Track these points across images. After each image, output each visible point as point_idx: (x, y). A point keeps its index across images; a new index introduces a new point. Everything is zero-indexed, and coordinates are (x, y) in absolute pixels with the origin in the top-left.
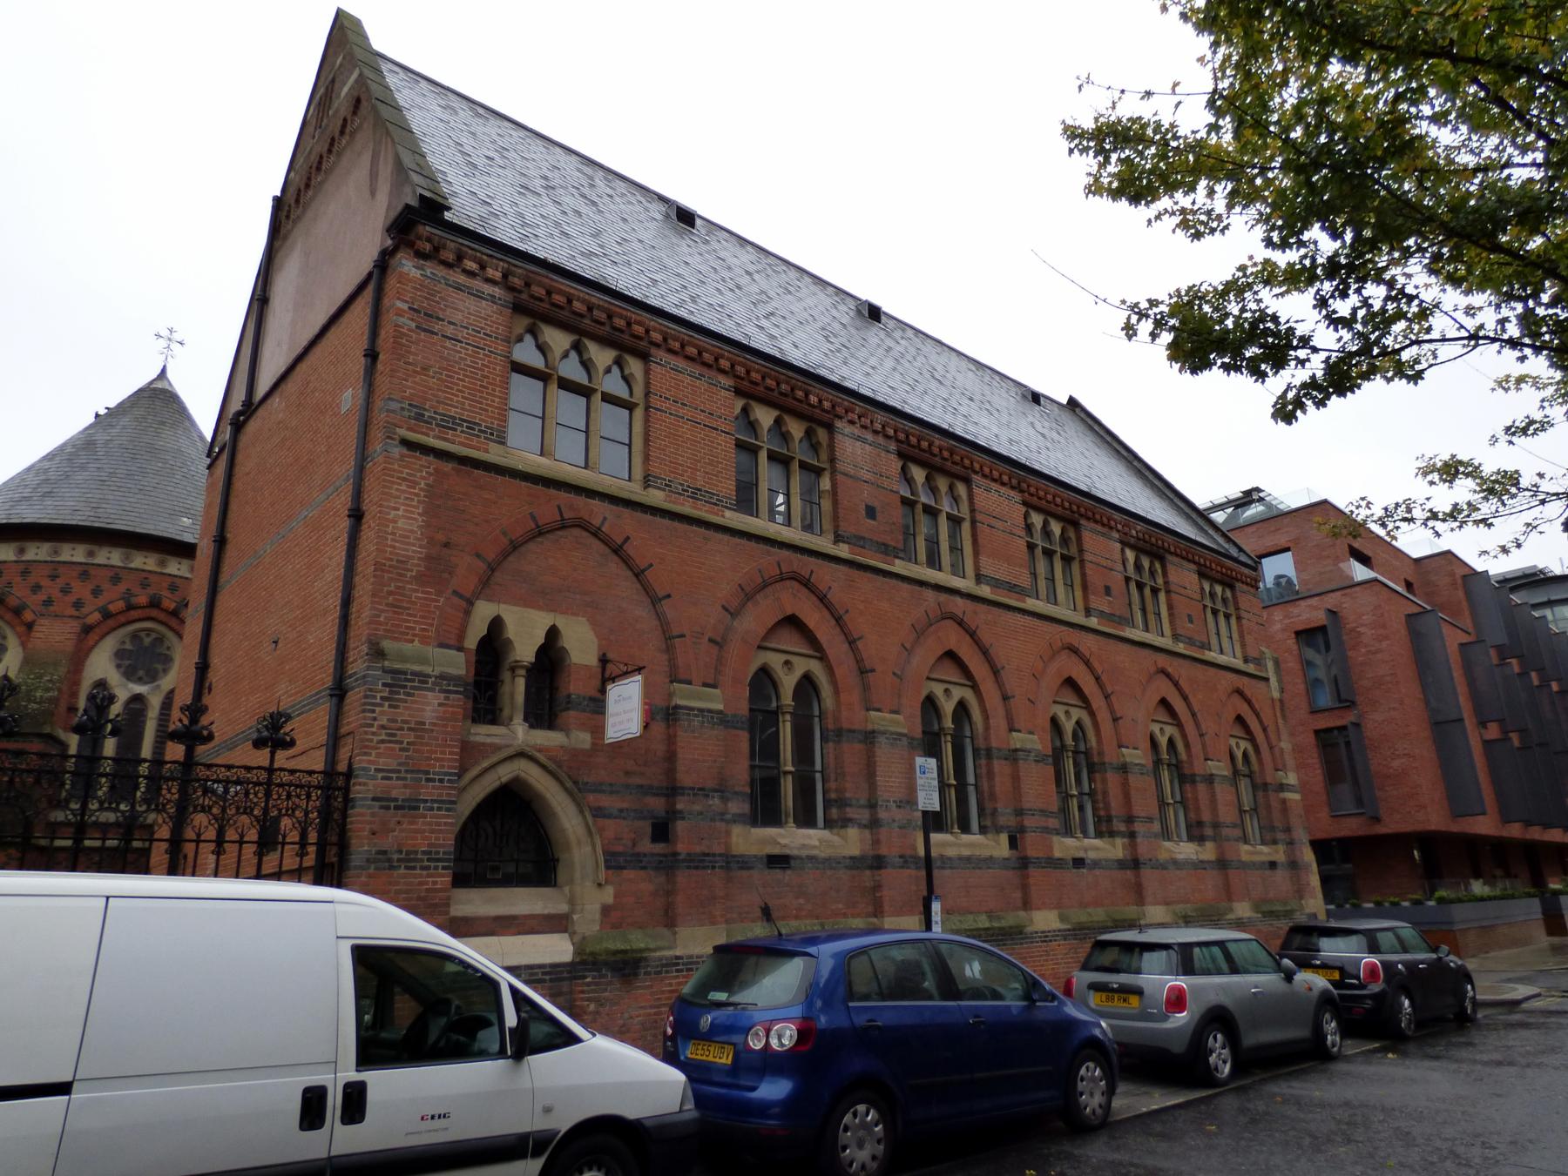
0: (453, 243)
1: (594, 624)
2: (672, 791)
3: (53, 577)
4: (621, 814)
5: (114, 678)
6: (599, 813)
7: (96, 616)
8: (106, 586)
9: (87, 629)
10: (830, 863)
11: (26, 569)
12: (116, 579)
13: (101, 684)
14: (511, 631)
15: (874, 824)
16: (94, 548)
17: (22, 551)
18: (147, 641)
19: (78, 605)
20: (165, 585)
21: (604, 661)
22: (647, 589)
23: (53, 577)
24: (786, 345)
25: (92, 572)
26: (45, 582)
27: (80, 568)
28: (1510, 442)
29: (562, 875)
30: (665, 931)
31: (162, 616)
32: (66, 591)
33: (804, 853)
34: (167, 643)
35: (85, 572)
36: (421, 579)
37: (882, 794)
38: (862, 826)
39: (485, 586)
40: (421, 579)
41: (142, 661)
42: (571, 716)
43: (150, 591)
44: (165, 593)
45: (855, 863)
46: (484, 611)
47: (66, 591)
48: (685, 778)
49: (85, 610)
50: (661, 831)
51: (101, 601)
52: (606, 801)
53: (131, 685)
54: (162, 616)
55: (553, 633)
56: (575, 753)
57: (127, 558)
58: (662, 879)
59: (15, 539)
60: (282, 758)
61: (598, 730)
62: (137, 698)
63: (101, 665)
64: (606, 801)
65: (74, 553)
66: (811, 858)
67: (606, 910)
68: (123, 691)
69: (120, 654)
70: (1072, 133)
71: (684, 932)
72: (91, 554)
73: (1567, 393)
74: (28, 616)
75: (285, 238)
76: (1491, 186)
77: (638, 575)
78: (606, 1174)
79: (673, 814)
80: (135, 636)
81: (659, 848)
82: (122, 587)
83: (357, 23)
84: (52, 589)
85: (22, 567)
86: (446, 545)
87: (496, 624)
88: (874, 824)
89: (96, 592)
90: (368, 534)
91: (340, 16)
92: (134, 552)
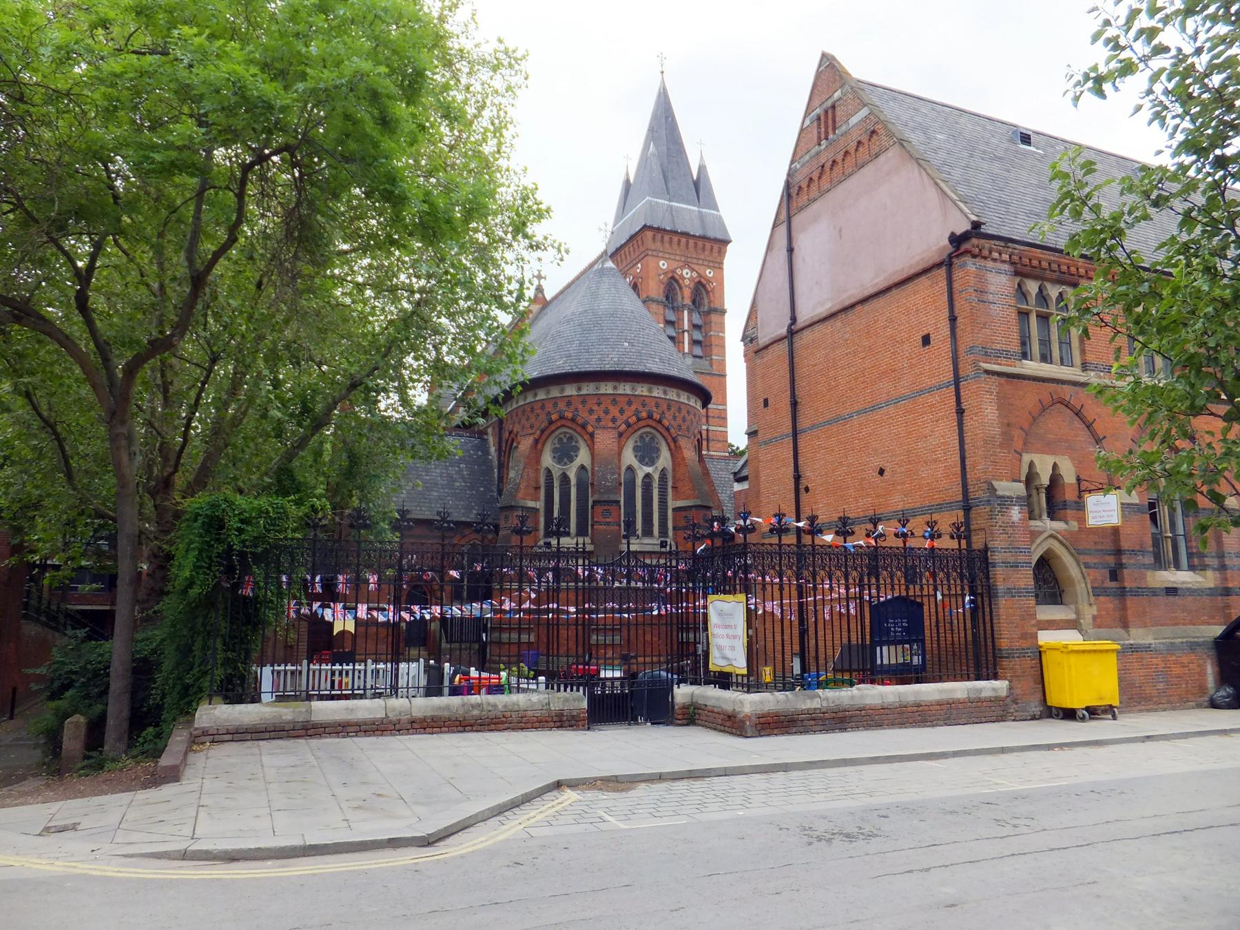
0: (987, 244)
1: (1072, 459)
2: (1118, 552)
3: (599, 404)
4: (1095, 567)
5: (635, 463)
6: (1087, 566)
7: (624, 426)
8: (626, 407)
9: (621, 435)
10: (1191, 592)
11: (584, 399)
12: (630, 403)
13: (630, 469)
14: (1038, 468)
15: (1223, 568)
16: (616, 384)
17: (579, 389)
18: (647, 439)
19: (614, 420)
21: (1078, 479)
22: (1094, 434)
23: (599, 404)
26: (595, 408)
29: (1066, 598)
30: (1121, 631)
31: (654, 424)
33: (1184, 586)
35: (614, 399)
36: (1001, 446)
37: (1227, 549)
38: (1214, 569)
39: (1027, 446)
40: (1001, 446)
41: (647, 454)
42: (1070, 513)
45: (1212, 592)
46: (1027, 458)
47: (607, 412)
48: (1125, 545)
49: (618, 423)
50: (1114, 575)
51: (625, 417)
52: (1088, 559)
54: (654, 424)
55: (1055, 466)
56: (1071, 533)
57: (650, 390)
58: (1117, 602)
61: (1082, 520)
62: (648, 476)
63: (629, 457)
64: (1088, 559)
65: (607, 388)
66: (1188, 589)
67: (1094, 618)
69: (636, 449)
71: (1133, 631)
72: (615, 388)
74: (590, 429)
75: (652, 130)
77: (1089, 426)
79: (1120, 566)
80: (641, 437)
81: (1114, 584)
83: (834, 58)
86: (1008, 425)
87: (1031, 465)
88: (1223, 568)
89: (622, 411)
90: (969, 423)
91: (824, 55)
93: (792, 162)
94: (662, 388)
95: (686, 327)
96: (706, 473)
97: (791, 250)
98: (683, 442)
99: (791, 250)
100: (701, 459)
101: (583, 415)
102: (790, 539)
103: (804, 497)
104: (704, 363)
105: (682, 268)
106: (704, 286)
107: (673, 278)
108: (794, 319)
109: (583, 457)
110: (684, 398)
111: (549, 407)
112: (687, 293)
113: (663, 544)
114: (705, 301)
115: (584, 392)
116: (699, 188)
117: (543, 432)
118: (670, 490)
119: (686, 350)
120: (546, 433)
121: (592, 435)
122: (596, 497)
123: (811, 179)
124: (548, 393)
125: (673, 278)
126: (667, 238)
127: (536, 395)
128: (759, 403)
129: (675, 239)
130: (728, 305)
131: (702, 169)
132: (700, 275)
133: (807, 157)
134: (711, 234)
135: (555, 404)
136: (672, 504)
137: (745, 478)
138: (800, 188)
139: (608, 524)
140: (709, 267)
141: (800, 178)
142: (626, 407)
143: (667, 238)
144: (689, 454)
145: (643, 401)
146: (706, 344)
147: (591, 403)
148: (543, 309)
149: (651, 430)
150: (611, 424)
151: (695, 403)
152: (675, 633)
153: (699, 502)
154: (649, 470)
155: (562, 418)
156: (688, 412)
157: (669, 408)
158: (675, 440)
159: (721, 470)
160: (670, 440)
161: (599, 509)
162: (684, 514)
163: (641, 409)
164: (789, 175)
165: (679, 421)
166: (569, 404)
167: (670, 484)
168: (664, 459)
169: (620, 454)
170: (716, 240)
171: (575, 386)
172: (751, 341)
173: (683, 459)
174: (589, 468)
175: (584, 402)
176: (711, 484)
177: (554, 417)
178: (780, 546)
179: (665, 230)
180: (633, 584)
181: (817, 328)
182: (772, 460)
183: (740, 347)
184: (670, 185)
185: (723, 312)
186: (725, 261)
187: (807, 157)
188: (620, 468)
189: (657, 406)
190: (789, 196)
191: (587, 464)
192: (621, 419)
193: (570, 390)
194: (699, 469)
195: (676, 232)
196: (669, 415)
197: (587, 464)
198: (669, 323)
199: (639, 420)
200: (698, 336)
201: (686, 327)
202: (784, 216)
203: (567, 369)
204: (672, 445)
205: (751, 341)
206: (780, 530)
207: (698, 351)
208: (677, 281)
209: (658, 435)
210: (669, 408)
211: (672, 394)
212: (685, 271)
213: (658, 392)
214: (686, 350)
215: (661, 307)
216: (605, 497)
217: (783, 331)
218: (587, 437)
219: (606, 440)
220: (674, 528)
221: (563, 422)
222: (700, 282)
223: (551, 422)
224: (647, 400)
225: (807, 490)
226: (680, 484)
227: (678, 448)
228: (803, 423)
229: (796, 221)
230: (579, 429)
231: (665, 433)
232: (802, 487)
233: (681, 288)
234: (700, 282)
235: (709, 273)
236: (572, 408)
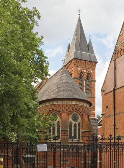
3: (63, 106)
5: (72, 121)
7: (69, 112)
8: (70, 107)
9: (68, 114)
11: (59, 105)
13: (71, 122)
17: (57, 102)
18: (75, 115)
19: (67, 110)
20: (77, 106)
24: (118, 65)
26: (62, 107)
28: (35, 8)
31: (77, 111)
32: (65, 108)
41: (75, 118)
47: (65, 108)
49: (68, 111)
51: (69, 110)
54: (77, 111)
60: (103, 141)
62: (75, 124)
63: (70, 119)
65: (65, 102)
69: (72, 117)
70: (27, 2)
73: (1, 57)
74: (60, 112)
76: (77, 115)
82: (72, 107)
84: (63, 108)
85: (58, 105)
92: (73, 101)
93: (116, 45)
94: (79, 102)
95: (85, 85)
96: (90, 123)
97: (115, 68)
98: (84, 116)
99: (115, 68)
100: (89, 119)
101: (59, 109)
102: (112, 141)
103: (116, 130)
104: (90, 95)
105: (84, 70)
106: (90, 74)
107: (81, 72)
108: (115, 86)
109: (59, 119)
110: (85, 104)
111: (50, 107)
112: (85, 76)
113: (79, 140)
114: (90, 78)
115: (59, 103)
116: (89, 48)
117: (48, 113)
118: (81, 127)
119: (85, 91)
120: (49, 114)
121: (61, 114)
122: (62, 129)
123: (121, 49)
124: (49, 103)
125: (81, 72)
126: (80, 61)
127: (46, 104)
128: (105, 107)
129: (82, 61)
130: (96, 79)
131: (90, 42)
132: (89, 72)
133: (121, 43)
134: (92, 60)
135: (51, 106)
136: (81, 131)
137: (101, 125)
138: (118, 51)
139: (65, 136)
140: (91, 69)
141: (118, 49)
142: (70, 107)
143: (80, 61)
144: (86, 119)
145: (74, 105)
146: (90, 89)
147: (61, 106)
148: (47, 81)
149: (76, 113)
150: (66, 111)
151: (88, 106)
152: (81, 161)
153: (88, 131)
154: (76, 122)
155: (53, 110)
156: (86, 108)
157: (81, 107)
158: (82, 115)
159: (94, 122)
160: (81, 115)
161: (63, 132)
162: (84, 133)
163: (74, 107)
164: (115, 48)
165: (84, 110)
166: (55, 106)
167: (81, 126)
168: (80, 120)
169: (68, 119)
170: (94, 62)
171: (56, 102)
172: (104, 91)
173: (85, 120)
174: (60, 122)
175: (59, 106)
176: (91, 126)
177: (51, 109)
178: (111, 143)
179: (79, 59)
180: (50, 150)
181: (121, 88)
182: (108, 121)
183: (100, 93)
184: (81, 47)
185: (95, 81)
186: (96, 68)
187: (121, 43)
188: (68, 122)
189: (78, 107)
190: (115, 54)
191: (60, 121)
192: (68, 110)
193: (55, 103)
194: (88, 123)
195: (83, 60)
196: (81, 109)
197: (60, 121)
198: (80, 84)
199: (73, 110)
200: (88, 87)
201: (85, 85)
202: (113, 59)
203: (54, 97)
204: (82, 116)
205: (104, 91)
206: (110, 139)
207: (88, 91)
208: (82, 73)
209: (78, 114)
210: (81, 107)
211: (82, 104)
212: (85, 70)
213: (78, 103)
214: (85, 91)
215: (78, 80)
216: (64, 129)
217: (112, 89)
218: (60, 114)
219: (64, 115)
220: (82, 137)
221: (53, 111)
222: (89, 73)
223: (50, 111)
224: (75, 105)
225: (117, 128)
226: (83, 126)
227: (83, 117)
228: (117, 112)
229: (117, 60)
230: (57, 112)
231: (80, 114)
232: (116, 128)
233: (84, 75)
234: (89, 73)
235: (91, 71)
236: (56, 107)
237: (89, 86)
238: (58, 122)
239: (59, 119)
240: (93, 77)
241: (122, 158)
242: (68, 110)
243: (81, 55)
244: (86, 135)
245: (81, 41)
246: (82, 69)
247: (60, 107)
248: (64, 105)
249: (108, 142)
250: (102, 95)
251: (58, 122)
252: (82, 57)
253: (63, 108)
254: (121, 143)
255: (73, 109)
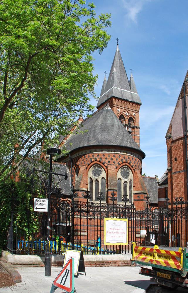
3: (109, 156)
5: (121, 178)
8: (118, 158)
9: (117, 167)
19: (114, 162)
25: (115, 155)
26: (108, 157)
27: (113, 154)
34: (94, 175)
41: (125, 175)
43: (125, 159)
44: (128, 159)
47: (112, 159)
49: (116, 163)
51: (118, 161)
53: (124, 179)
59: (94, 148)
62: (126, 182)
63: (119, 175)
68: (124, 180)
78: (147, 291)
85: (103, 154)
89: (117, 159)
117: (89, 165)
125: (122, 115)
132: (131, 115)
136: (133, 192)
142: (118, 158)
150: (113, 164)
162: (137, 195)
163: (123, 159)
165: (136, 164)
177: (93, 160)
178: (181, 208)
191: (105, 177)
192: (117, 162)
197: (105, 177)
203: (97, 143)
220: (134, 200)
223: (92, 162)
224: (126, 156)
237: (132, 133)
238: (131, 180)
239: (103, 174)
240: (137, 122)
241: (133, 225)
242: (117, 162)
243: (122, 94)
244: (139, 197)
245: (121, 75)
246: (123, 110)
247: (105, 157)
248: (110, 155)
249: (84, 202)
250: (167, 143)
251: (103, 178)
252: (122, 96)
253: (109, 159)
254: (81, 202)
255: (122, 160)
